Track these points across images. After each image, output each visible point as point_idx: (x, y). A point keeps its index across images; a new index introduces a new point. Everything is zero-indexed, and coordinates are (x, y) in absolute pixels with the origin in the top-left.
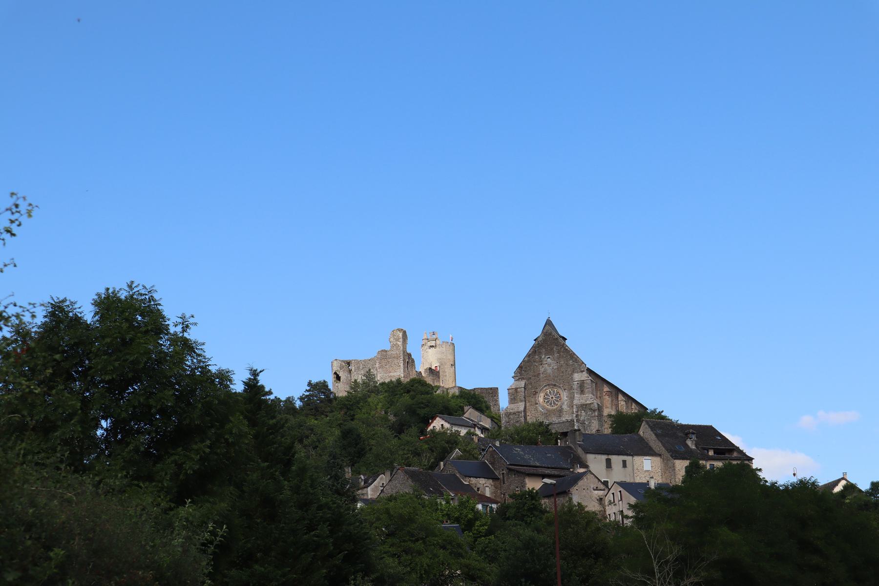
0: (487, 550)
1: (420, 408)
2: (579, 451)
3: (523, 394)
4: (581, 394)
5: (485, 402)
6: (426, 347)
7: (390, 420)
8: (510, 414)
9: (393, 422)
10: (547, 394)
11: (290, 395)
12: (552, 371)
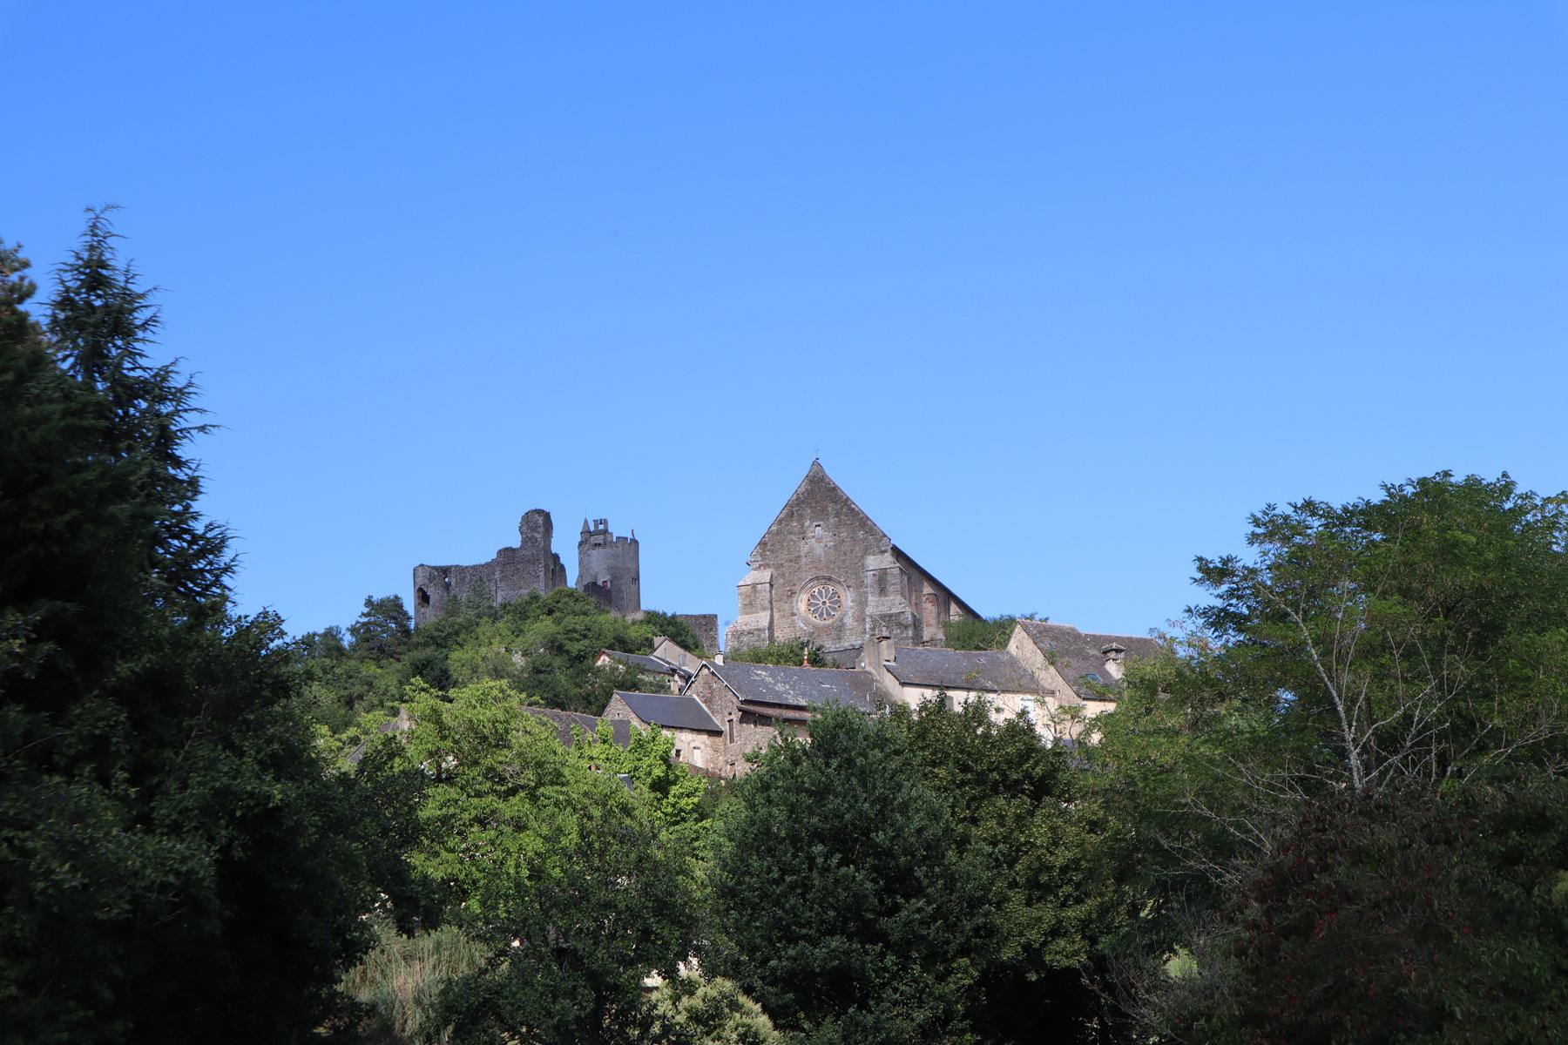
1: (571, 640)
2: (887, 681)
3: (768, 595)
4: (880, 595)
5: (693, 637)
6: (587, 547)
7: (514, 664)
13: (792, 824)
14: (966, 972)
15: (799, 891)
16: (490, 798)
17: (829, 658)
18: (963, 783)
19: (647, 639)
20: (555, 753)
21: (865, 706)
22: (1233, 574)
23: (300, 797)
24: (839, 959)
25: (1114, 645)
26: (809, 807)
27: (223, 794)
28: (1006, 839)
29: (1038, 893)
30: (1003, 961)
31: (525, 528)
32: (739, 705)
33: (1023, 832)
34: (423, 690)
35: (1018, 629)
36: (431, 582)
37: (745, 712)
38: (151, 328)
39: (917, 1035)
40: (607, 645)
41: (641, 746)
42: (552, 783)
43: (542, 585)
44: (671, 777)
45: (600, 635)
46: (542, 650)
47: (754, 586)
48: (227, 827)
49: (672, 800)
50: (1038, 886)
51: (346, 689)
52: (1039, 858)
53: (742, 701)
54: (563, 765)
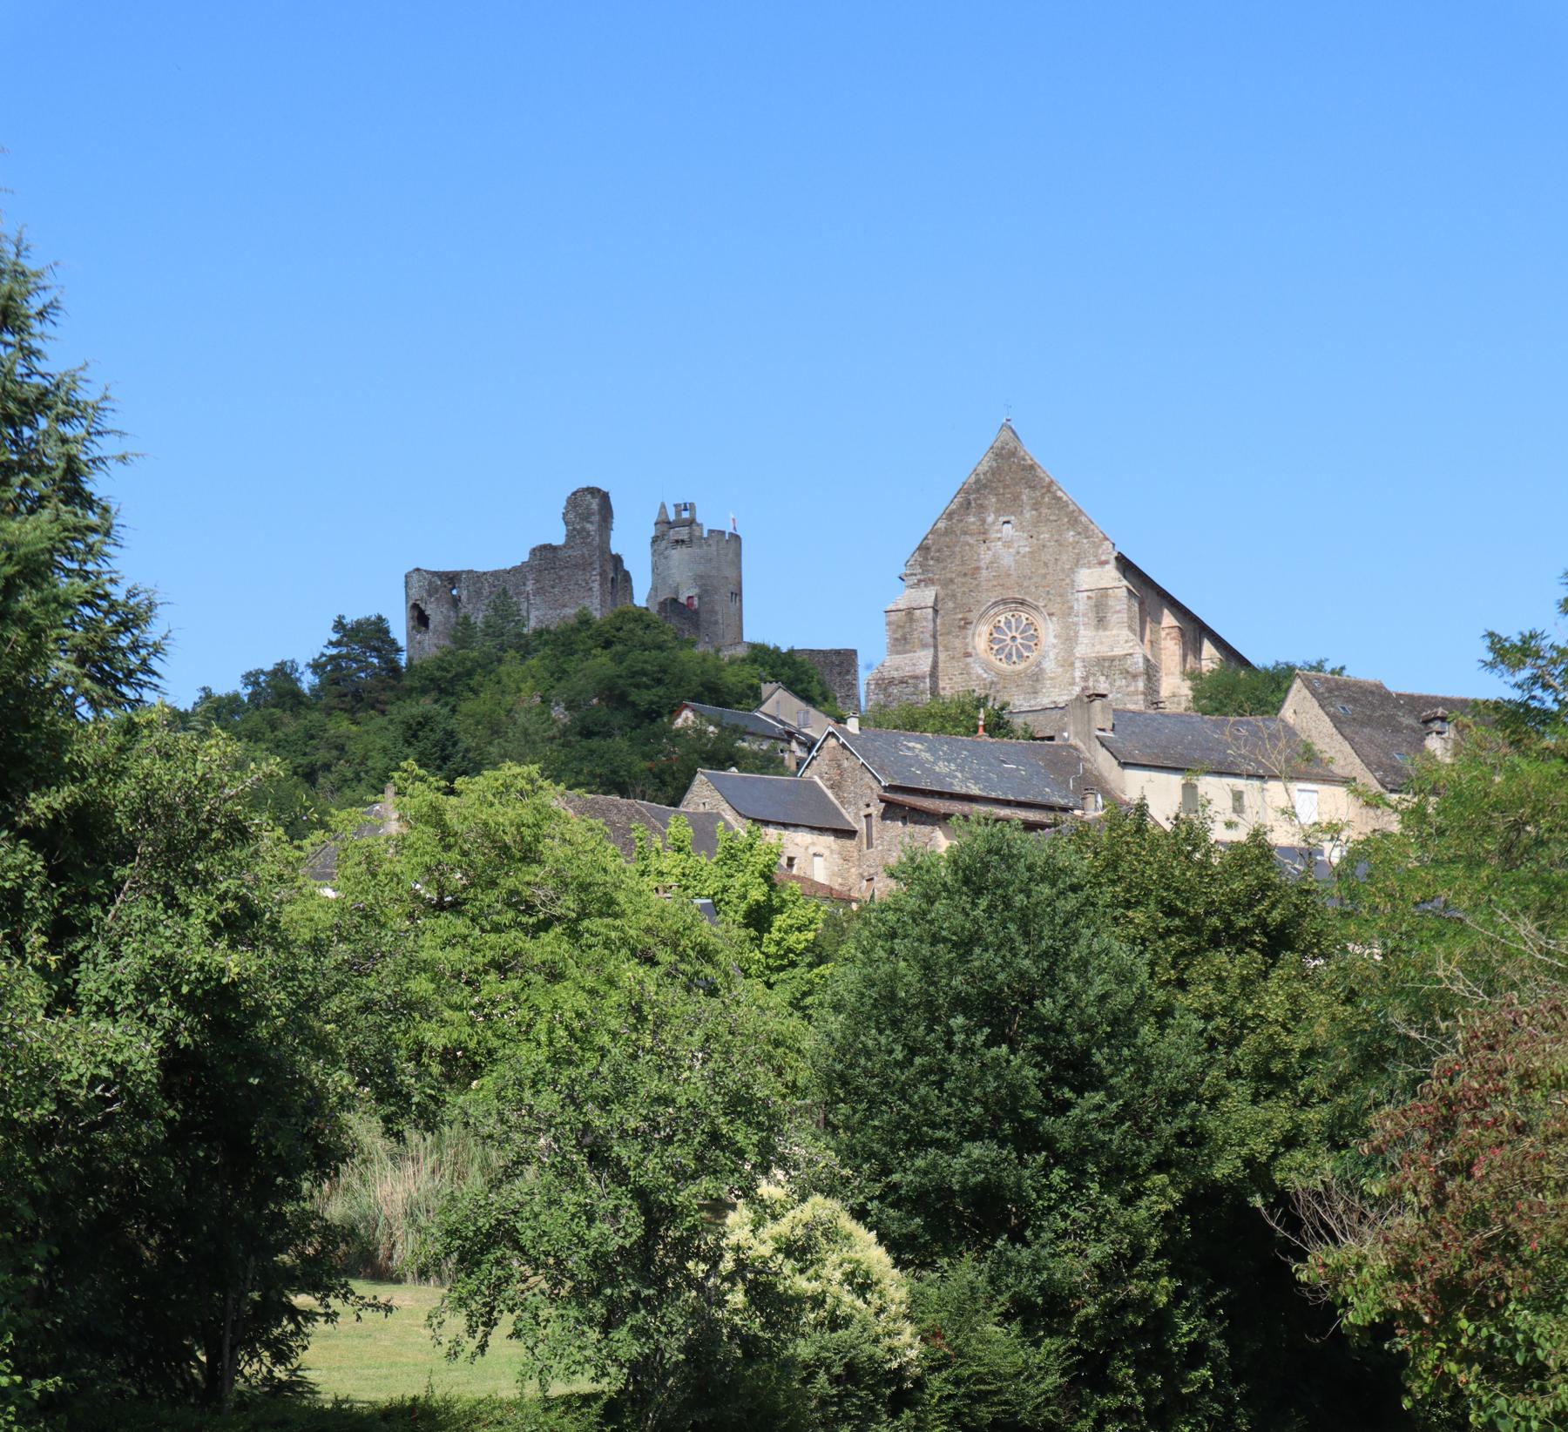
0: (808, 1000)
1: (638, 686)
2: (1100, 759)
3: (931, 626)
5: (821, 683)
8: (891, 682)
9: (565, 725)
10: (997, 628)
11: (287, 658)
12: (1016, 562)
13: (925, 986)
14: (1162, 1193)
15: (933, 1078)
16: (513, 933)
17: (1018, 722)
18: (1168, 932)
19: (751, 687)
20: (605, 870)
21: (1066, 797)
22: (1538, 655)
23: (261, 968)
24: (986, 1172)
25: (1440, 711)
26: (949, 964)
27: (167, 963)
28: (1225, 1011)
29: (1268, 1087)
30: (1216, 1180)
31: (571, 516)
32: (882, 792)
33: (1250, 1002)
34: (422, 779)
35: (1297, 684)
36: (430, 596)
37: (889, 804)
38: (52, 317)
39: (1092, 1278)
40: (691, 695)
41: (733, 857)
42: (601, 915)
43: (597, 601)
44: (776, 902)
45: (681, 679)
46: (595, 701)
47: (910, 611)
48: (170, 1006)
49: (776, 935)
50: (1270, 1077)
51: (305, 754)
52: (1270, 1037)
53: (885, 787)
54: (617, 887)
